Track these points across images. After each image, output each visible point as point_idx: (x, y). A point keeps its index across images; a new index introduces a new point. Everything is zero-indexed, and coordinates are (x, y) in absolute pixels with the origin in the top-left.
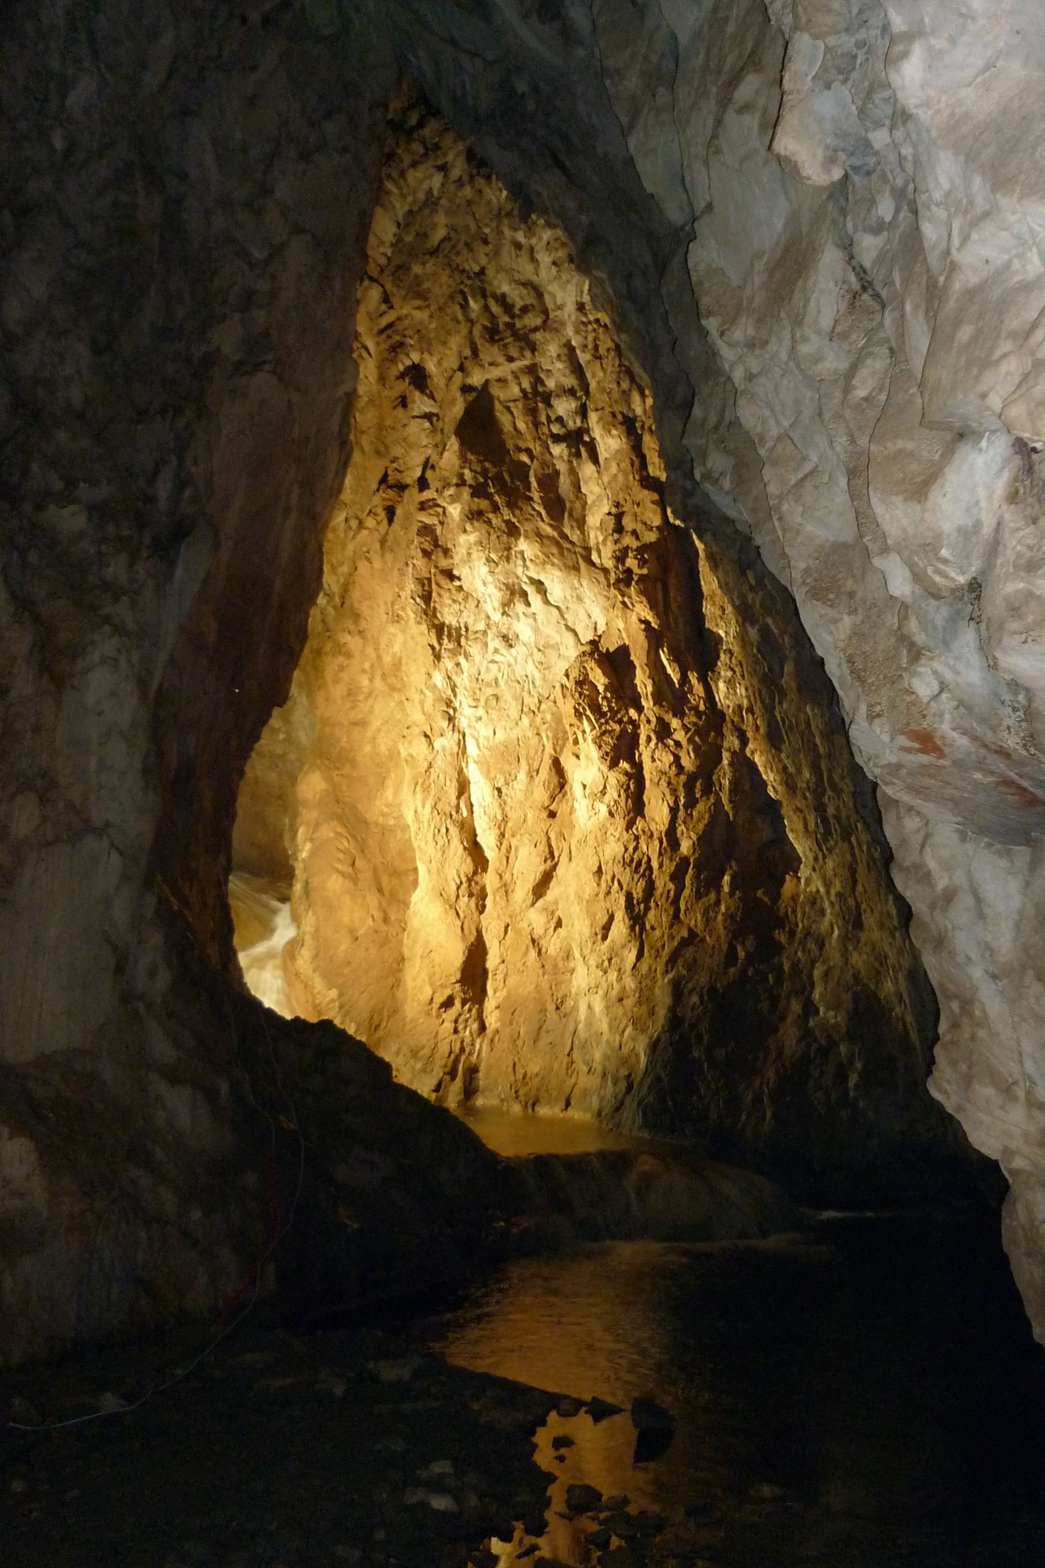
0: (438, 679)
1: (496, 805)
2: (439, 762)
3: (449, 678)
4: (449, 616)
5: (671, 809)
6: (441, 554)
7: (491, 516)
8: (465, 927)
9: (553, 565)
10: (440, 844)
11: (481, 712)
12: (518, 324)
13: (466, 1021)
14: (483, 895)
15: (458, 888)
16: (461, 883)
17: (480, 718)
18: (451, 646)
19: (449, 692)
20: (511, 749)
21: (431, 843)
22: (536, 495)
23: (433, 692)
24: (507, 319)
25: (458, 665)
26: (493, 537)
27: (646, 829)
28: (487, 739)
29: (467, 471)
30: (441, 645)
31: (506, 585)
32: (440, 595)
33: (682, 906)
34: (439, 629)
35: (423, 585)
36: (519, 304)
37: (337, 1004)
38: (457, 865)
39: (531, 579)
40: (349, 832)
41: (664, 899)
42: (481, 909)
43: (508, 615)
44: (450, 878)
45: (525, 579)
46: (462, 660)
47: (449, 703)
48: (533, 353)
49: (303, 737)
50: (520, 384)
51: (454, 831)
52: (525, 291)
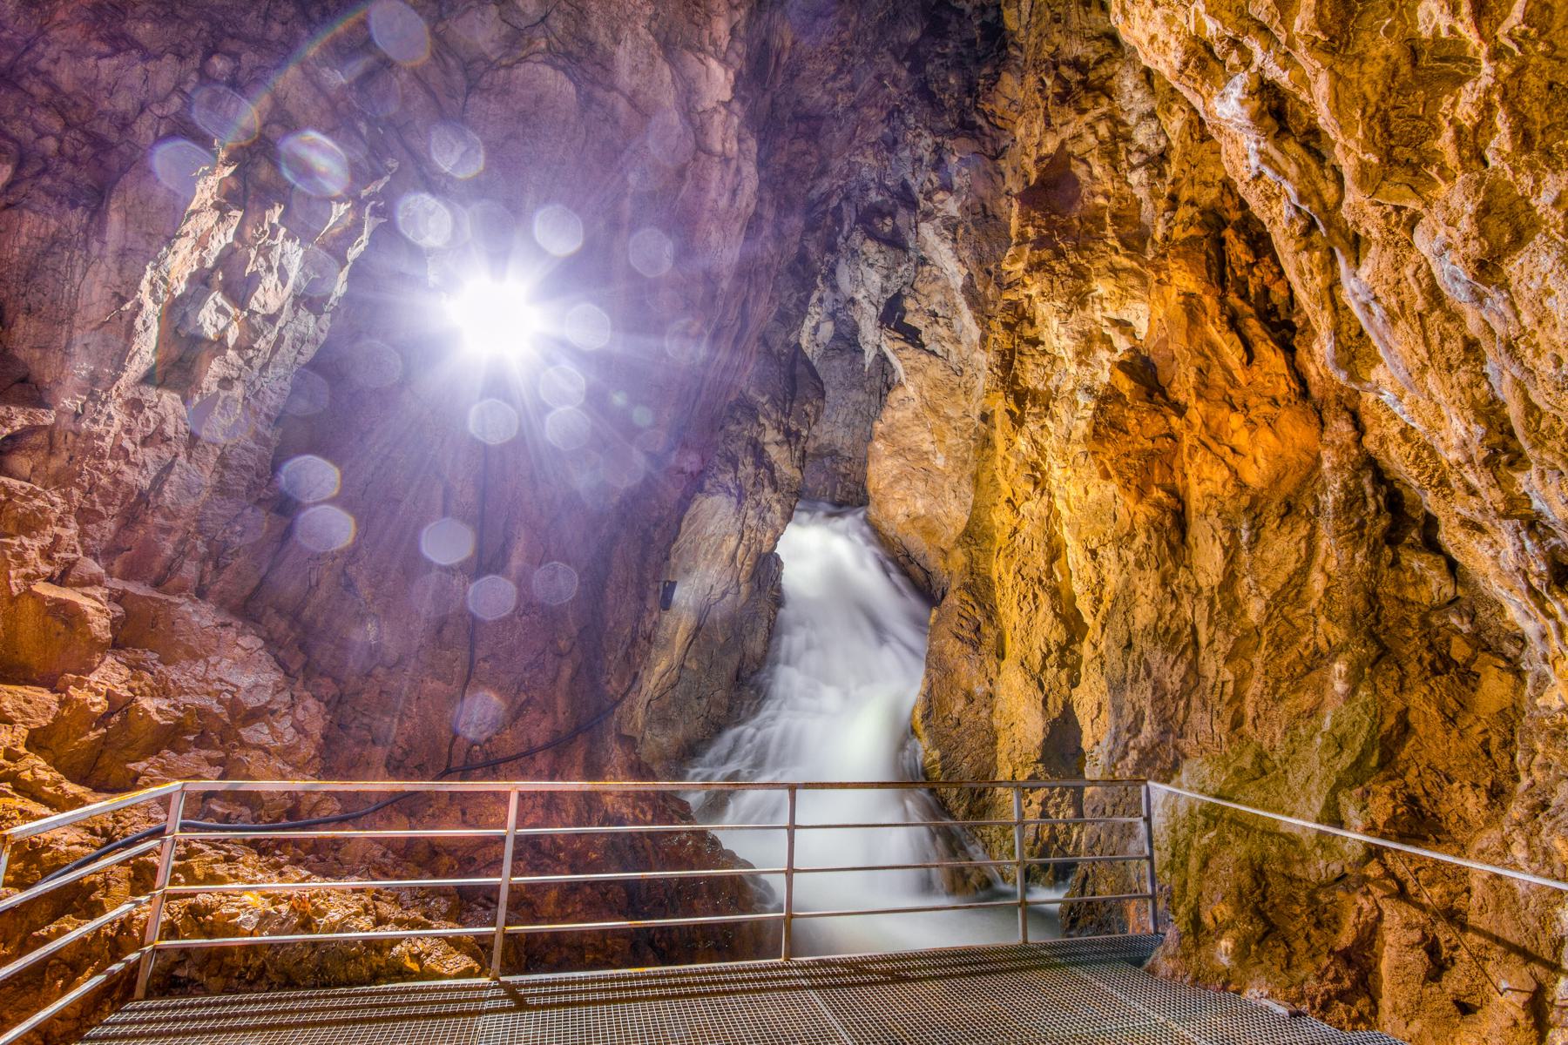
0: (1022, 443)
1: (1089, 568)
2: (1026, 528)
3: (1035, 442)
4: (1031, 378)
5: (1226, 550)
6: (1026, 324)
7: (1053, 263)
8: (1050, 701)
9: (1134, 298)
10: (1026, 609)
11: (1069, 472)
12: (1092, 76)
13: (1057, 806)
14: (1075, 667)
15: (1045, 657)
16: (1050, 652)
17: (1068, 479)
18: (1036, 410)
19: (1036, 456)
20: (1106, 508)
21: (1016, 610)
22: (1109, 232)
23: (1016, 457)
24: (1079, 77)
25: (1043, 427)
26: (1057, 284)
27: (1193, 584)
28: (1079, 500)
29: (1030, 229)
30: (1022, 410)
31: (1083, 334)
32: (1021, 363)
33: (1249, 712)
34: (1020, 396)
35: (1004, 355)
36: (1093, 57)
37: (939, 766)
38: (1046, 632)
39: (1109, 319)
40: (976, 600)
41: (1216, 697)
42: (1074, 682)
43: (1088, 365)
44: (1035, 646)
45: (1105, 323)
46: (1048, 422)
47: (1035, 467)
48: (1111, 98)
49: (640, 461)
50: (1096, 133)
51: (1044, 598)
52: (1098, 44)
